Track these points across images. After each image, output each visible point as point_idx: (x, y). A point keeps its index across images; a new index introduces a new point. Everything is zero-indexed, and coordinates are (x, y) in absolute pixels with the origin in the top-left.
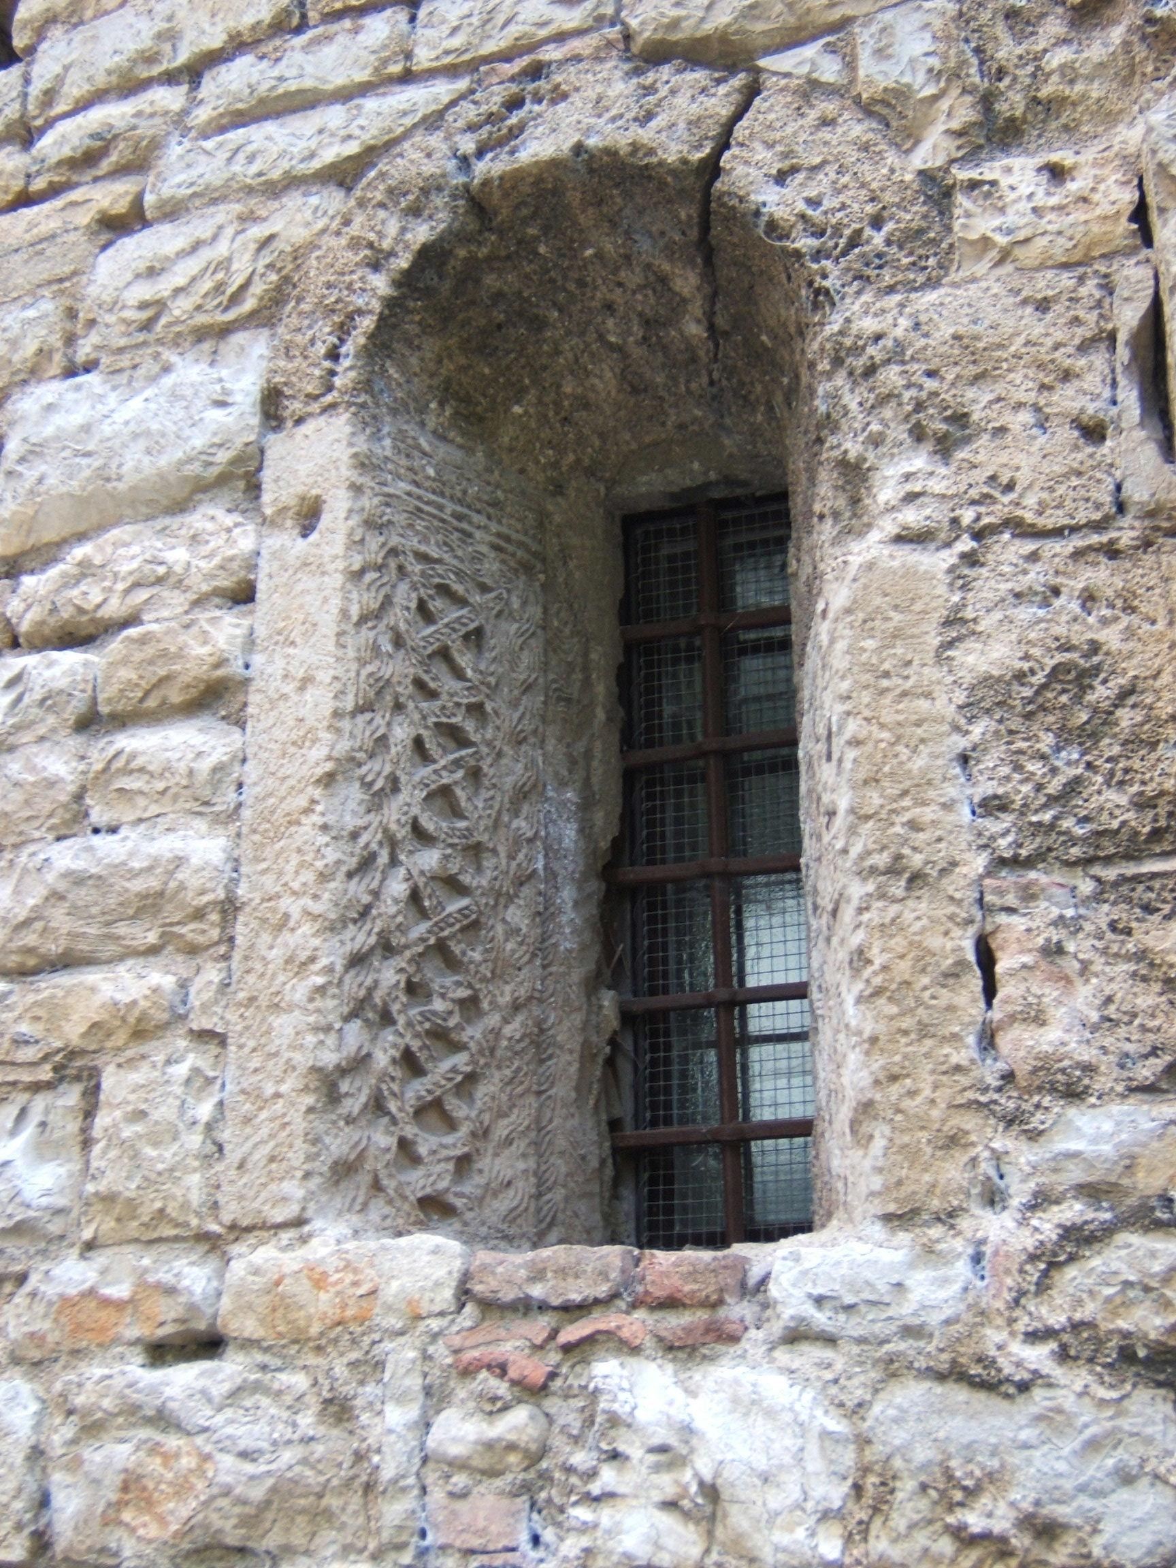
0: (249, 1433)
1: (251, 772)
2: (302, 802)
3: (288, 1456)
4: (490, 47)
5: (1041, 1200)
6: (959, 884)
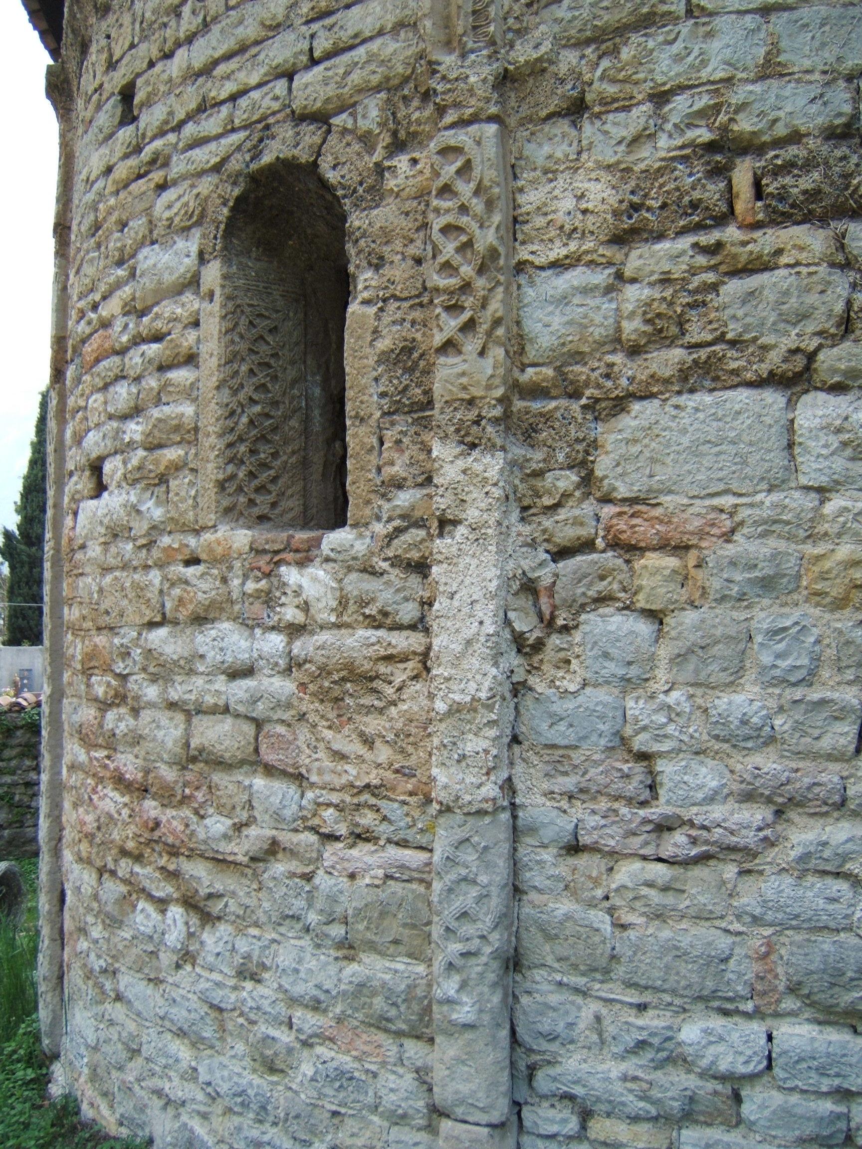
0: (204, 586)
1: (201, 385)
2: (211, 395)
3: (213, 593)
4: (255, 118)
5: (390, 519)
6: (372, 422)
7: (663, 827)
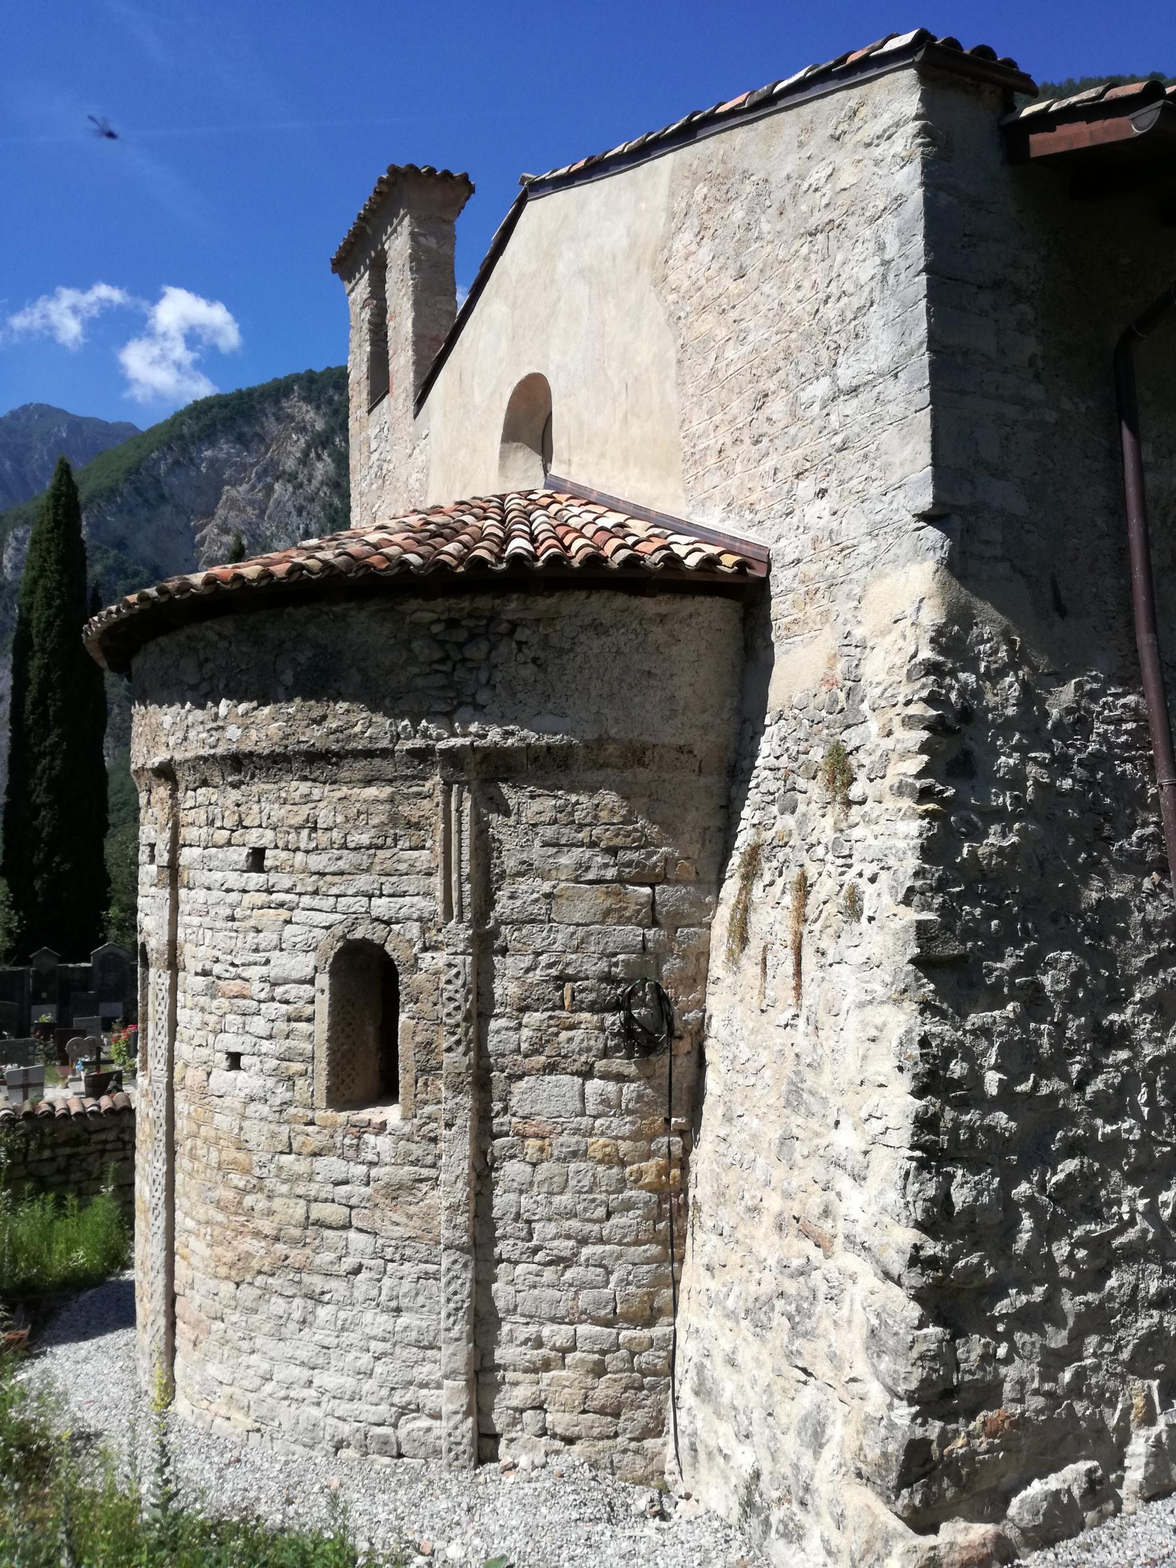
7: (535, 1251)
